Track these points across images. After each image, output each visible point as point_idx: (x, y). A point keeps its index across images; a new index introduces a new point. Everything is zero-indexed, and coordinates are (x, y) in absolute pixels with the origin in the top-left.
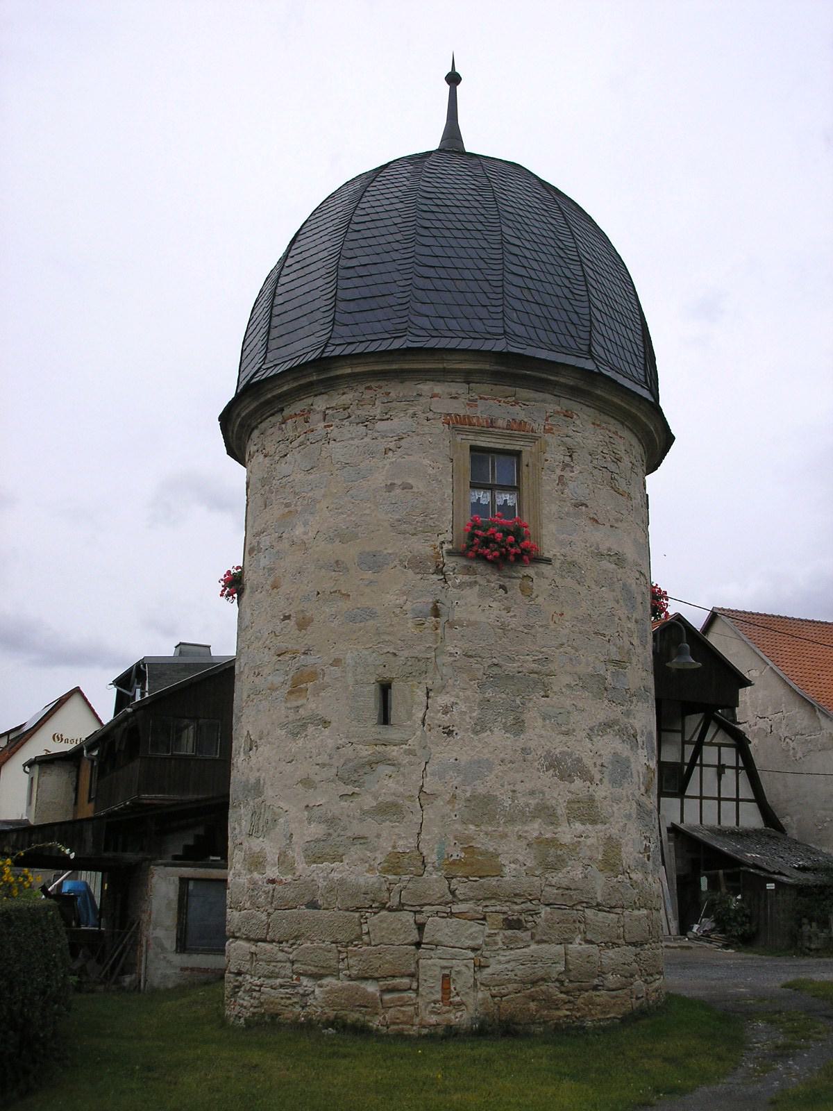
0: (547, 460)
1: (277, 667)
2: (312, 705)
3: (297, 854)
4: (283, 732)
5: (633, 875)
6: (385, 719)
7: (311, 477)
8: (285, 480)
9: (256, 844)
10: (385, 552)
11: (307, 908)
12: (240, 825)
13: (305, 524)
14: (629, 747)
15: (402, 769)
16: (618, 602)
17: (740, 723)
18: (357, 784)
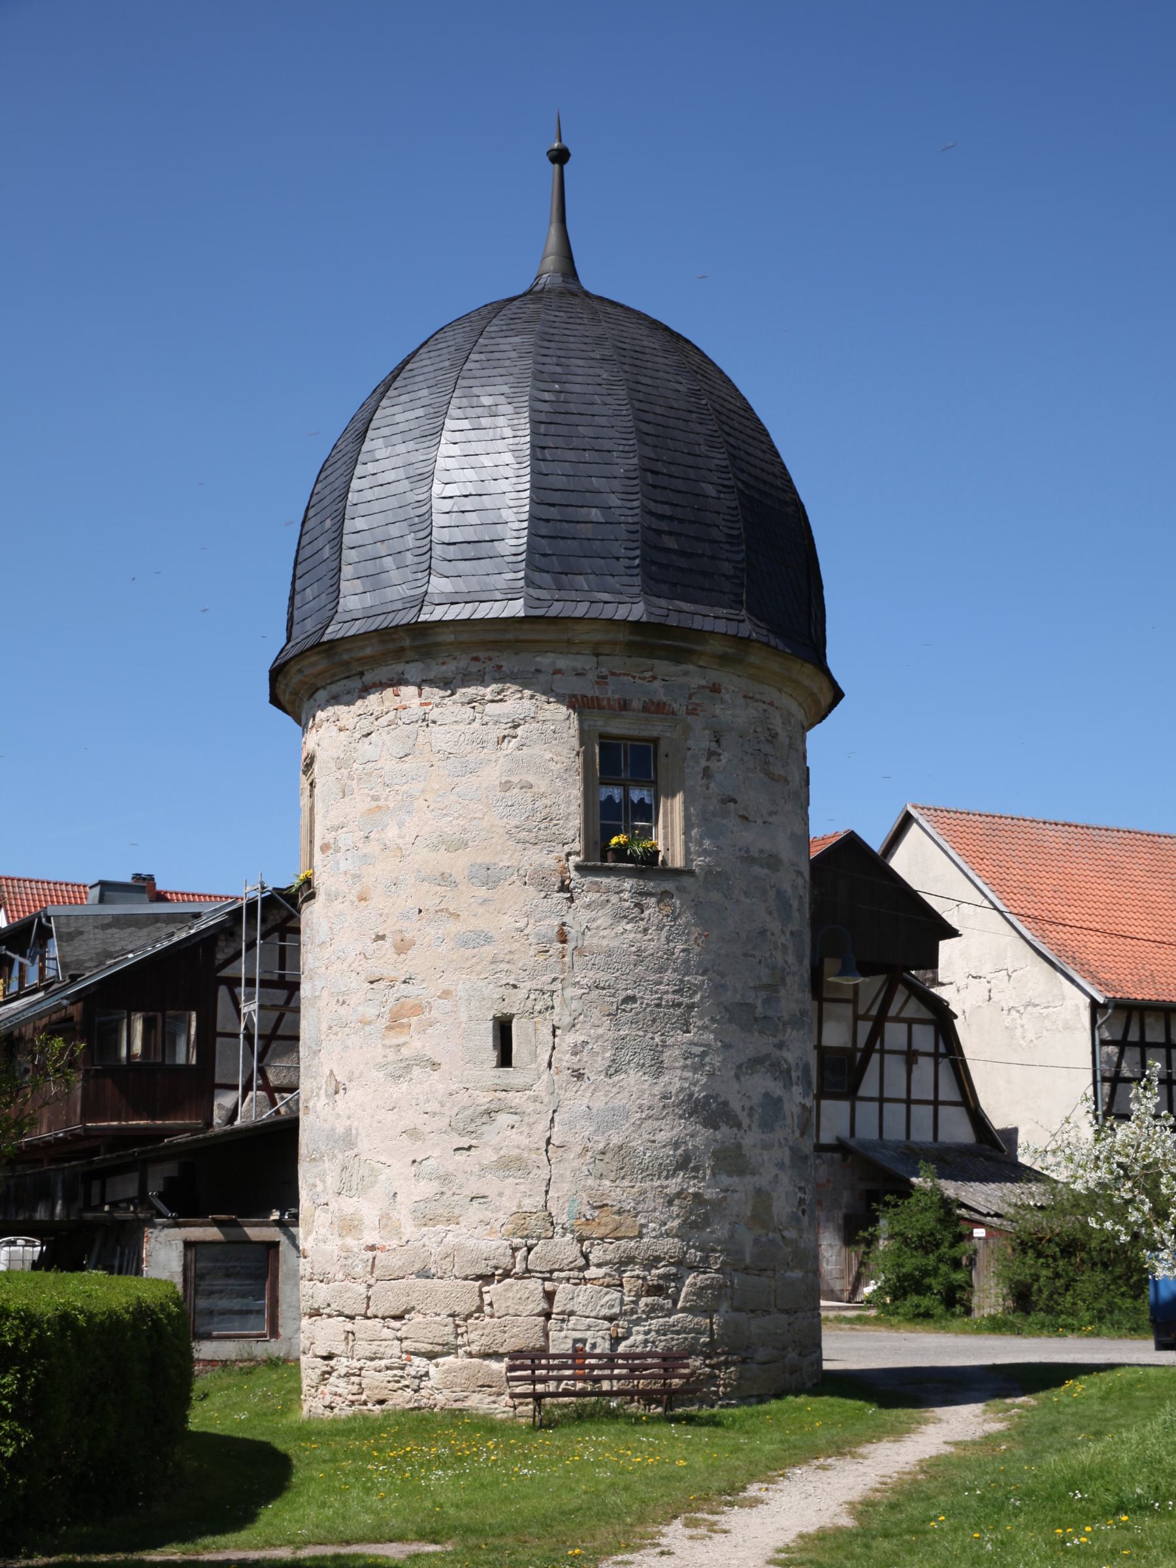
0: (689, 749)
1: (369, 997)
2: (416, 1044)
3: (403, 1216)
4: (381, 1075)
5: (785, 1233)
6: (505, 1059)
7: (406, 766)
8: (370, 765)
9: (348, 1205)
10: (501, 864)
11: (418, 1277)
12: (324, 1182)
13: (401, 825)
14: (781, 1084)
15: (526, 1118)
16: (770, 914)
17: (942, 984)
18: (474, 1135)
